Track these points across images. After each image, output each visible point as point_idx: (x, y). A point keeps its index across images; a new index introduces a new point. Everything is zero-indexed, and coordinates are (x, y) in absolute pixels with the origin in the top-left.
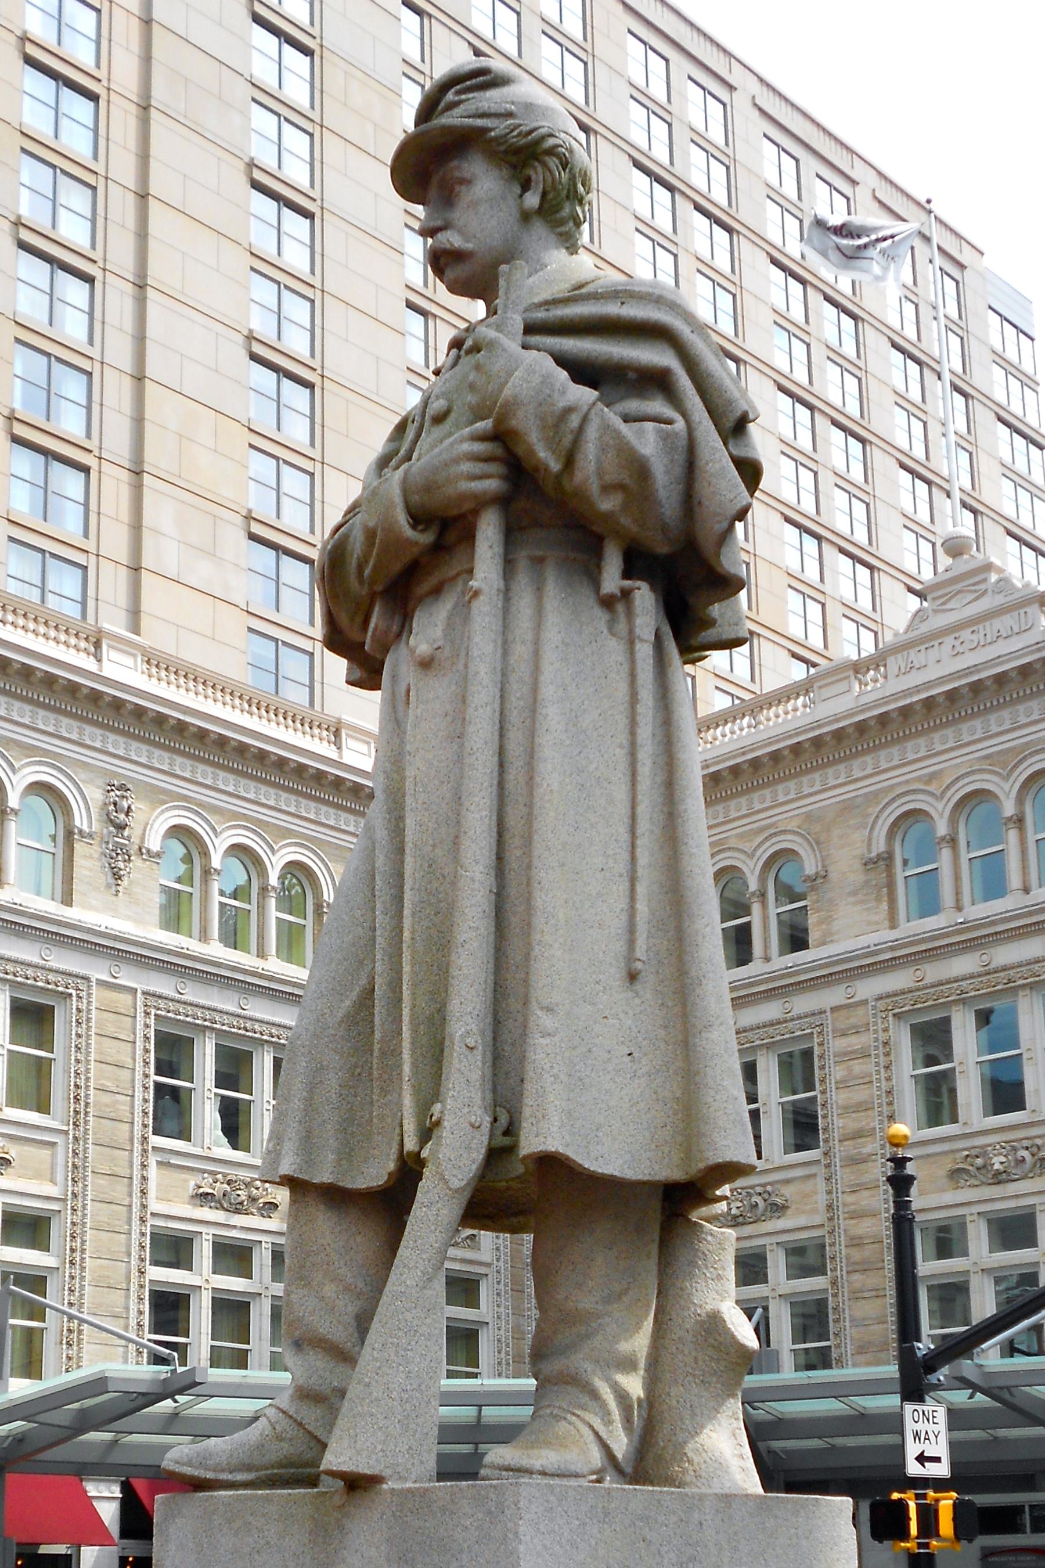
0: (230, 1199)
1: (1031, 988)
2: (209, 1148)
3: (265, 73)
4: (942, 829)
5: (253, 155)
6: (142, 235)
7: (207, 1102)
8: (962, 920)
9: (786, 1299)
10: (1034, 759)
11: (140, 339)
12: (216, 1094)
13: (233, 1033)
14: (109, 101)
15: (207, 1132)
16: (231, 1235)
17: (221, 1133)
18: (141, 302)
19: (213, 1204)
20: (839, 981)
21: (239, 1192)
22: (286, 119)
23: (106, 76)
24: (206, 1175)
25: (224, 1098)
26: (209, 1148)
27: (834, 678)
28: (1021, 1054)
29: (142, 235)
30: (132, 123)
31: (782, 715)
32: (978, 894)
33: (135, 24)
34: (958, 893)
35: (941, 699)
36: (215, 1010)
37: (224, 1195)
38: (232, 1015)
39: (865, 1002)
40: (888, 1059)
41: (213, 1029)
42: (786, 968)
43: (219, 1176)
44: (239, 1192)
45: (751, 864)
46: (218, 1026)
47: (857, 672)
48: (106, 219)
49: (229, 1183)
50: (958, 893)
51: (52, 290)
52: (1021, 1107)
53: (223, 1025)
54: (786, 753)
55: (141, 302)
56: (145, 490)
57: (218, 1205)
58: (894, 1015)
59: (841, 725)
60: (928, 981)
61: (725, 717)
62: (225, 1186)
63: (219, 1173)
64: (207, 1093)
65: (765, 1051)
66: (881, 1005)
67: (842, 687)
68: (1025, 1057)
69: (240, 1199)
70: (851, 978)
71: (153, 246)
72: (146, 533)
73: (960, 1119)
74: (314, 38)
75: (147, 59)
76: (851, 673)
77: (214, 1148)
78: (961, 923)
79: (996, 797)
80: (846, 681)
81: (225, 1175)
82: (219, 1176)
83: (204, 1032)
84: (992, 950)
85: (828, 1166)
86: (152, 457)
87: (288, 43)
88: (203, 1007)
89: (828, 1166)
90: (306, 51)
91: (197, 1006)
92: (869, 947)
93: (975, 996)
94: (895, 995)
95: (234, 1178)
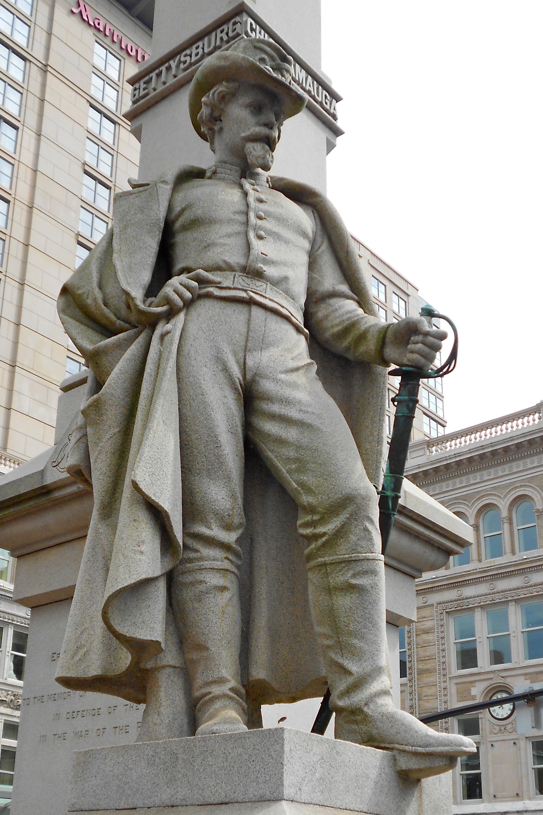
0: (14, 703)
1: (515, 602)
2: (6, 679)
3: (88, 196)
4: (504, 513)
5: (79, 230)
6: (25, 262)
7: (7, 658)
8: (434, 577)
9: (529, 740)
10: (484, 499)
11: (20, 307)
12: (12, 654)
13: (22, 626)
14: (14, 204)
15: (5, 672)
16: (13, 720)
17: (13, 672)
18: (21, 291)
19: (5, 705)
20: (454, 588)
21: (19, 700)
22: (96, 216)
23: (14, 193)
24: (3, 691)
25: (16, 656)
26: (6, 679)
27: (418, 448)
28: (476, 640)
29: (25, 262)
30: (25, 214)
31: (459, 445)
32: (489, 554)
33: (29, 172)
34: (479, 554)
35: (488, 454)
36: (14, 615)
37: (11, 701)
38: (22, 617)
39: (433, 605)
40: (410, 639)
41: (12, 623)
42: (432, 579)
43: (10, 692)
44: (19, 700)
45: (503, 503)
46: (15, 623)
47: (428, 446)
48: (8, 254)
49: (14, 695)
50: (479, 554)
51: (92, 225)
52: (476, 666)
53: (18, 622)
54: (442, 468)
55: (21, 291)
56: (16, 374)
57: (8, 706)
58: (446, 612)
59: (473, 455)
60: (531, 583)
61: (452, 437)
62: (12, 697)
63: (10, 691)
64: (7, 654)
65: (480, 609)
66: (440, 607)
67: (421, 453)
68: (478, 641)
69: (19, 704)
70: (425, 593)
71: (29, 267)
72: (15, 393)
73: (478, 665)
74: (112, 182)
75: (33, 187)
76: (426, 446)
77: (8, 679)
78: (525, 559)
79: (532, 499)
80: (423, 450)
81: (12, 692)
82: (10, 692)
83: (8, 625)
84: (529, 576)
85: (411, 686)
86: (21, 360)
87: (99, 183)
88: (8, 613)
89: (411, 686)
90: (108, 187)
91: (5, 613)
92: (476, 569)
93: (523, 598)
94: (447, 602)
95: (17, 694)
